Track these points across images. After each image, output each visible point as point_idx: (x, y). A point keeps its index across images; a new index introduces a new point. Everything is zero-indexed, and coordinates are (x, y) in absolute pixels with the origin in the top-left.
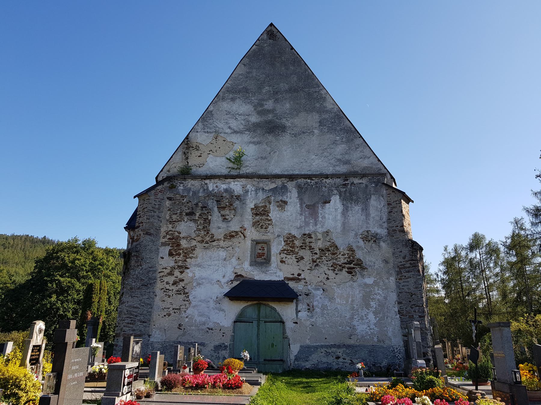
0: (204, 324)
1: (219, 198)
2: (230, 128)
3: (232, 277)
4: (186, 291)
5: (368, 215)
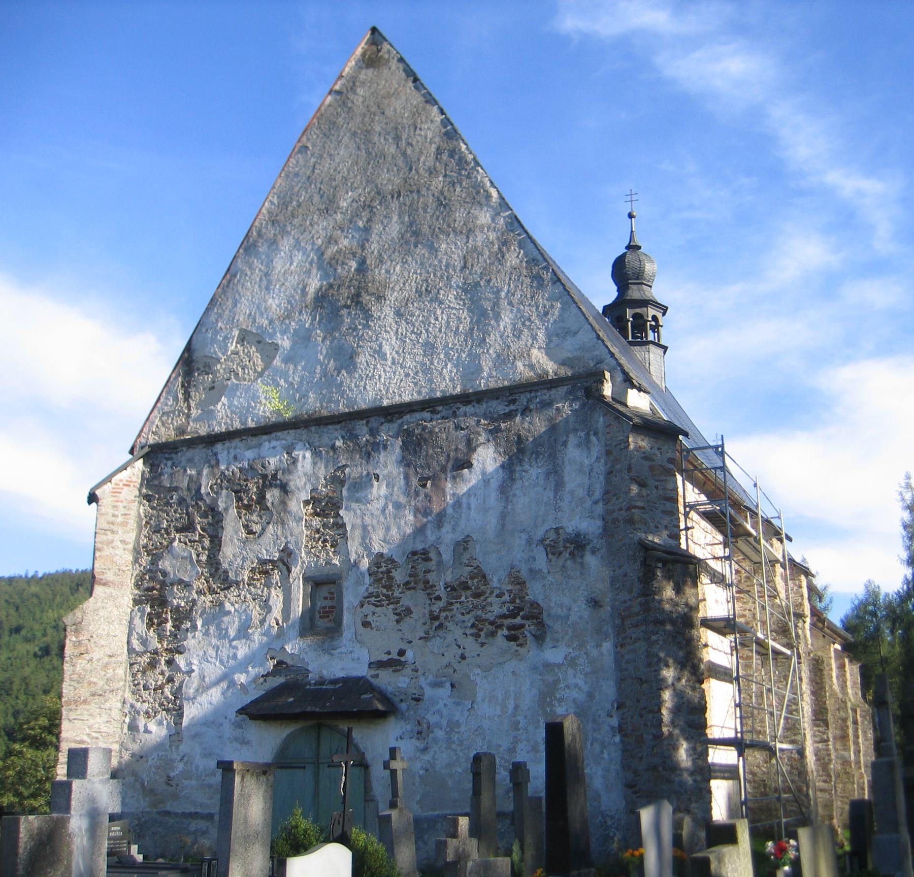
5: (559, 485)
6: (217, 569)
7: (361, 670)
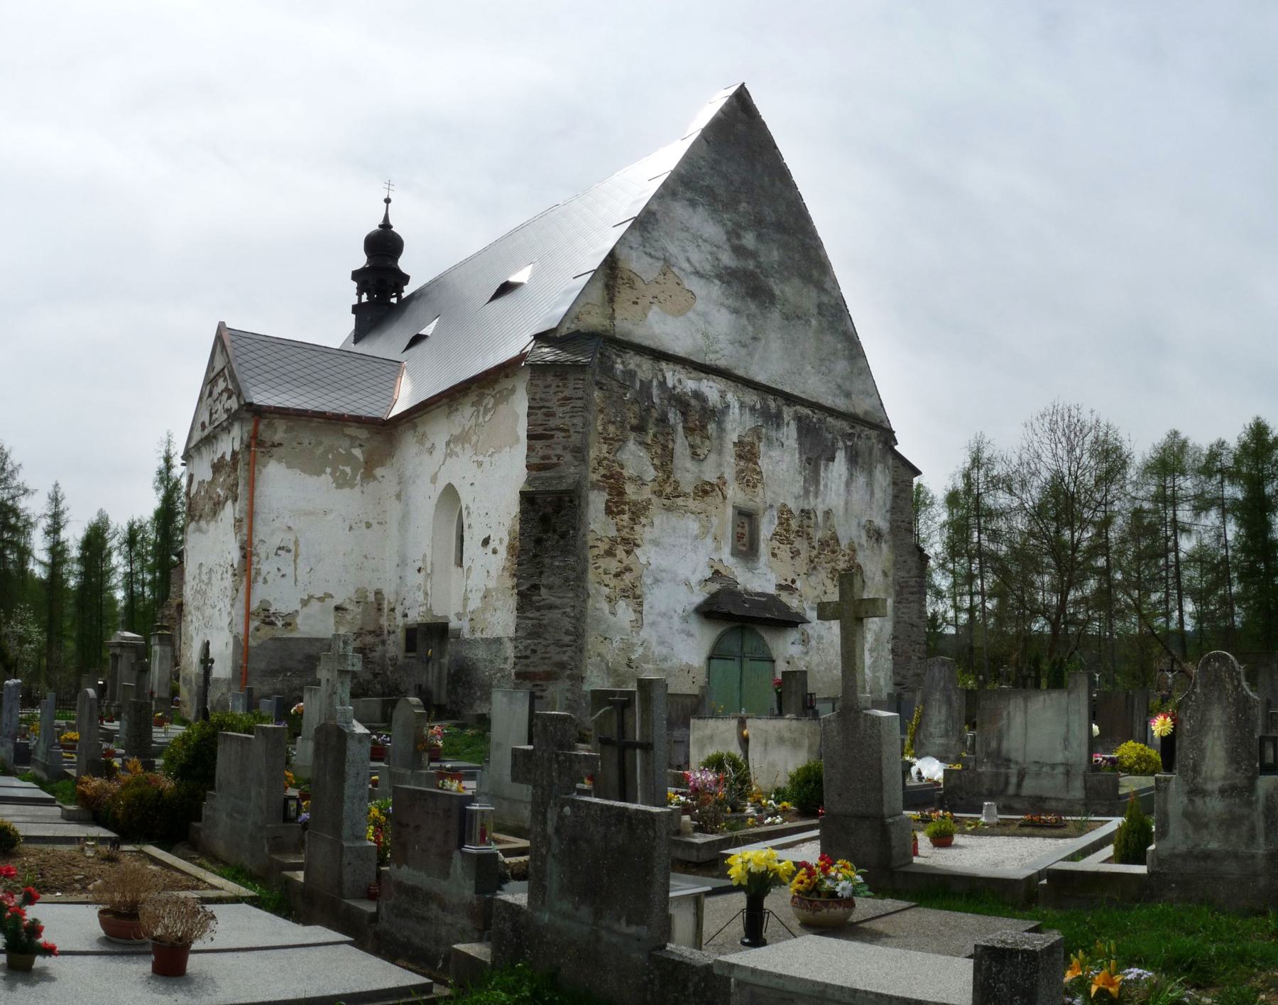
0: (665, 659)
1: (681, 402)
2: (688, 260)
3: (708, 574)
4: (638, 592)
5: (872, 494)
6: (668, 477)
7: (771, 590)
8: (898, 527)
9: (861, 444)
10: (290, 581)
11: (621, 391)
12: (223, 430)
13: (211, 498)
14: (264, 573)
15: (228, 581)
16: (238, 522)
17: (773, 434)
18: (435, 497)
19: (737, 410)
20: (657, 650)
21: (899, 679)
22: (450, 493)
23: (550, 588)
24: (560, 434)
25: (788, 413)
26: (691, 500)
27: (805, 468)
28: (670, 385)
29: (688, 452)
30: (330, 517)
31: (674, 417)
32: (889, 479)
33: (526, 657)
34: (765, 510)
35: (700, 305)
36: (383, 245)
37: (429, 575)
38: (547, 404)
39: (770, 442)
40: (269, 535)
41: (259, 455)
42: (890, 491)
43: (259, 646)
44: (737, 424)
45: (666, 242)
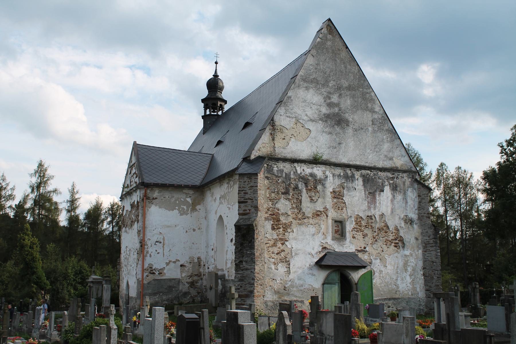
0: (302, 286)
1: (305, 180)
3: (320, 249)
5: (407, 202)
8: (422, 216)
9: (399, 181)
10: (161, 254)
11: (277, 179)
12: (134, 191)
13: (130, 219)
14: (150, 252)
15: (136, 256)
16: (139, 231)
17: (350, 185)
18: (217, 219)
19: (331, 178)
20: (298, 282)
21: (427, 288)
22: (221, 217)
23: (246, 262)
24: (249, 201)
25: (357, 174)
26: (311, 219)
27: (368, 197)
28: (299, 172)
29: (309, 199)
30: (178, 228)
31: (301, 186)
32: (416, 194)
33: (239, 289)
34: (348, 218)
35: (313, 134)
36: (214, 85)
37: (215, 252)
38: (245, 189)
39: (349, 189)
40: (151, 237)
41: (147, 203)
42: (417, 200)
43: (148, 283)
44: (332, 183)
45: (296, 110)
